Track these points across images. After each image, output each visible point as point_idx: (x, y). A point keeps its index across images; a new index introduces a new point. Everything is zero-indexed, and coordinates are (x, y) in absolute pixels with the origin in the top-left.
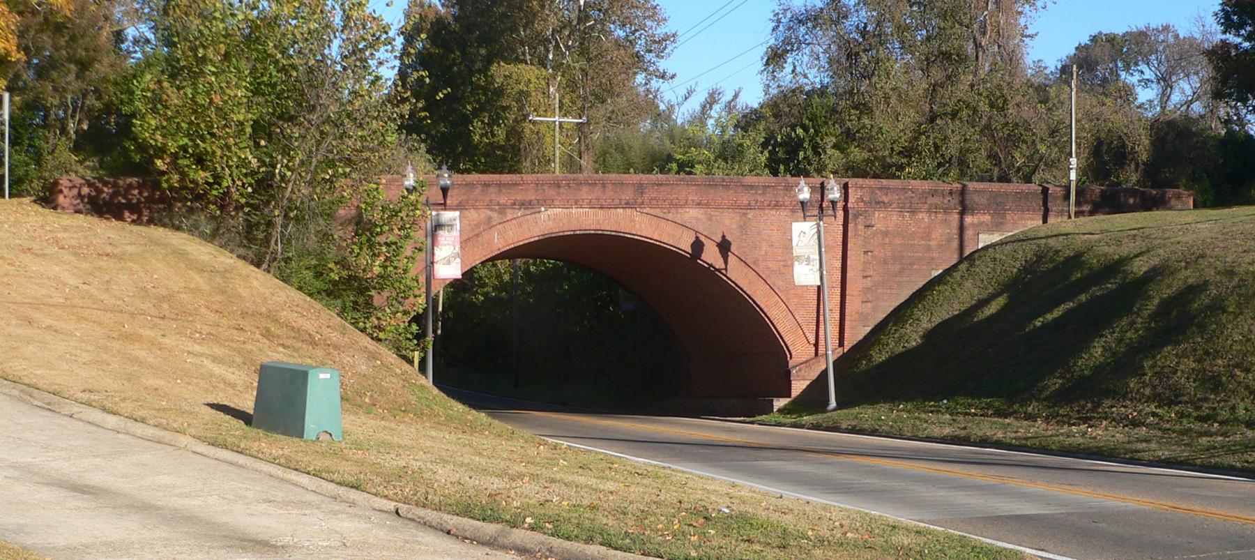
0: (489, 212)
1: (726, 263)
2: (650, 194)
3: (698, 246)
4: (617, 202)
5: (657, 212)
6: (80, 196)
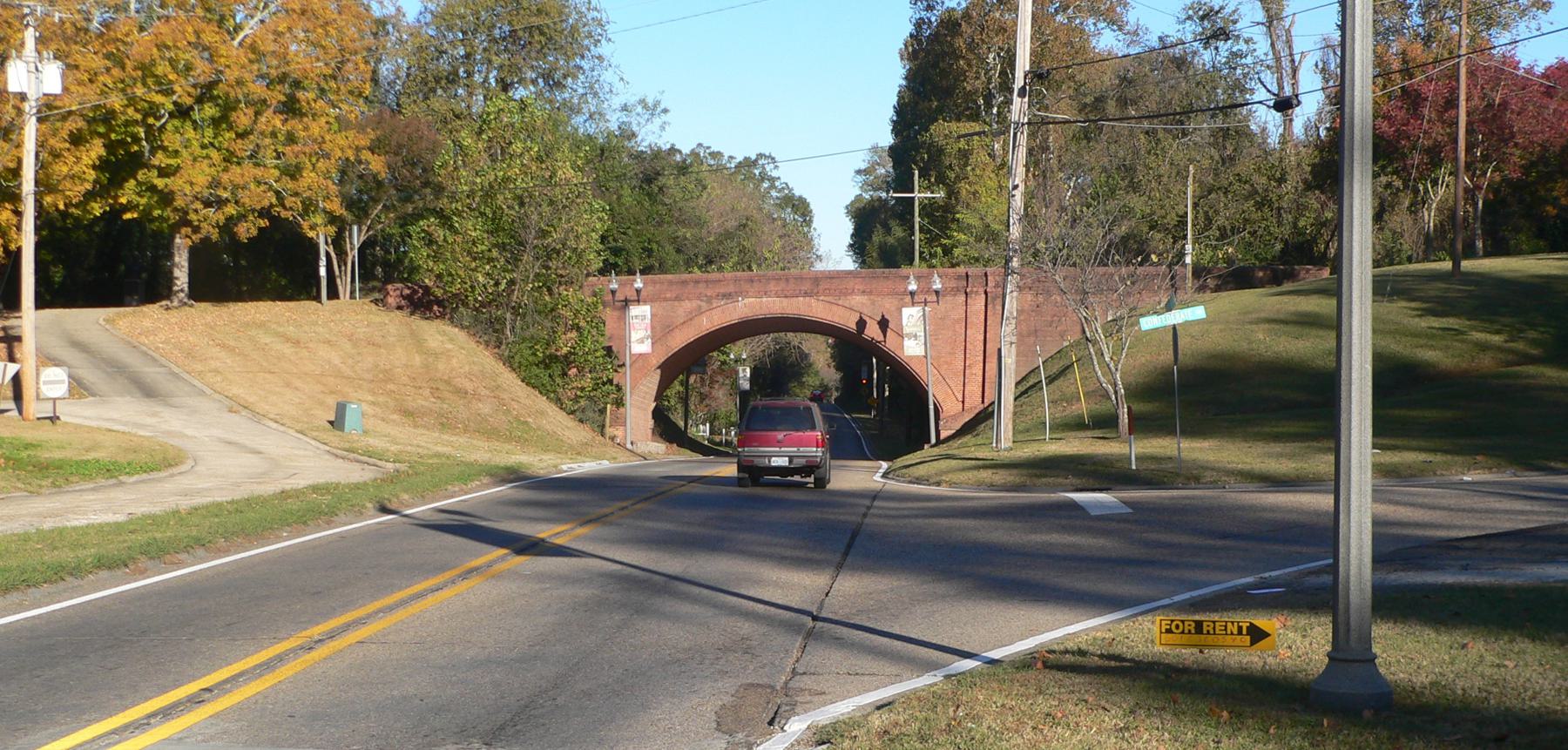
3: (861, 324)
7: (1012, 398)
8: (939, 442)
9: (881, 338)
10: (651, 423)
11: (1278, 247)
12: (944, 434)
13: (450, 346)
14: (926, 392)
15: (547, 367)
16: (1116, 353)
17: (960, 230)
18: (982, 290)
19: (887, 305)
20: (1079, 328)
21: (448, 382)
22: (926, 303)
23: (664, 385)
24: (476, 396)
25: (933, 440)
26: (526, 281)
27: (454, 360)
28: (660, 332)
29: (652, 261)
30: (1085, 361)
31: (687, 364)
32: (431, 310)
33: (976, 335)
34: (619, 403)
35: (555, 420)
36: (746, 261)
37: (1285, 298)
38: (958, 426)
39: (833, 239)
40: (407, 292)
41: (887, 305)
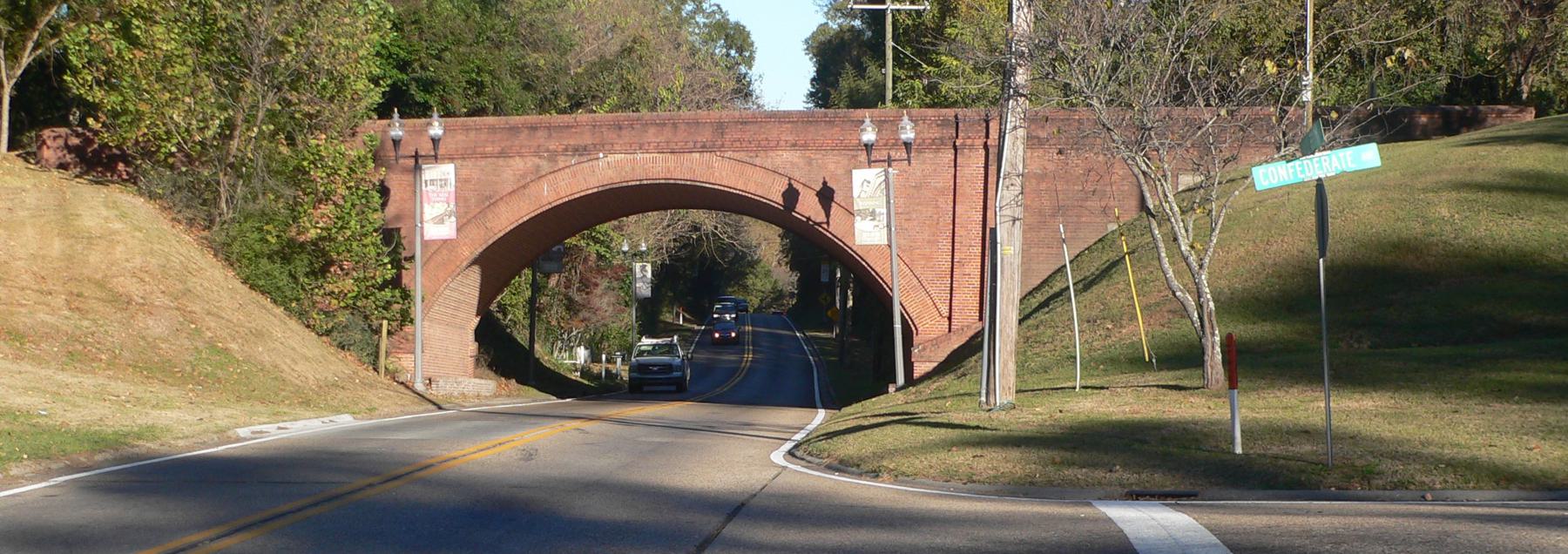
0: (537, 160)
1: (828, 215)
2: (732, 134)
3: (791, 195)
4: (691, 145)
5: (736, 155)
6: (67, 146)
7: (1014, 317)
8: (910, 381)
9: (821, 218)
10: (472, 347)
11: (1443, 81)
12: (920, 369)
13: (124, 227)
14: (891, 299)
15: (286, 259)
16: (1203, 234)
17: (950, 54)
18: (980, 142)
19: (829, 167)
20: (1136, 192)
21: (101, 285)
22: (889, 161)
23: (488, 292)
24: (147, 308)
25: (901, 380)
26: (249, 121)
27: (120, 248)
28: (469, 209)
29: (483, 101)
30: (1145, 253)
31: (531, 254)
32: (113, 170)
33: (970, 214)
34: (406, 318)
35: (292, 347)
36: (632, 99)
37: (1482, 150)
38: (942, 355)
39: (783, 78)
40: (75, 141)
41: (829, 167)
